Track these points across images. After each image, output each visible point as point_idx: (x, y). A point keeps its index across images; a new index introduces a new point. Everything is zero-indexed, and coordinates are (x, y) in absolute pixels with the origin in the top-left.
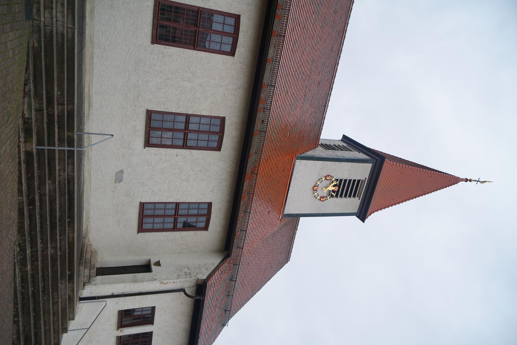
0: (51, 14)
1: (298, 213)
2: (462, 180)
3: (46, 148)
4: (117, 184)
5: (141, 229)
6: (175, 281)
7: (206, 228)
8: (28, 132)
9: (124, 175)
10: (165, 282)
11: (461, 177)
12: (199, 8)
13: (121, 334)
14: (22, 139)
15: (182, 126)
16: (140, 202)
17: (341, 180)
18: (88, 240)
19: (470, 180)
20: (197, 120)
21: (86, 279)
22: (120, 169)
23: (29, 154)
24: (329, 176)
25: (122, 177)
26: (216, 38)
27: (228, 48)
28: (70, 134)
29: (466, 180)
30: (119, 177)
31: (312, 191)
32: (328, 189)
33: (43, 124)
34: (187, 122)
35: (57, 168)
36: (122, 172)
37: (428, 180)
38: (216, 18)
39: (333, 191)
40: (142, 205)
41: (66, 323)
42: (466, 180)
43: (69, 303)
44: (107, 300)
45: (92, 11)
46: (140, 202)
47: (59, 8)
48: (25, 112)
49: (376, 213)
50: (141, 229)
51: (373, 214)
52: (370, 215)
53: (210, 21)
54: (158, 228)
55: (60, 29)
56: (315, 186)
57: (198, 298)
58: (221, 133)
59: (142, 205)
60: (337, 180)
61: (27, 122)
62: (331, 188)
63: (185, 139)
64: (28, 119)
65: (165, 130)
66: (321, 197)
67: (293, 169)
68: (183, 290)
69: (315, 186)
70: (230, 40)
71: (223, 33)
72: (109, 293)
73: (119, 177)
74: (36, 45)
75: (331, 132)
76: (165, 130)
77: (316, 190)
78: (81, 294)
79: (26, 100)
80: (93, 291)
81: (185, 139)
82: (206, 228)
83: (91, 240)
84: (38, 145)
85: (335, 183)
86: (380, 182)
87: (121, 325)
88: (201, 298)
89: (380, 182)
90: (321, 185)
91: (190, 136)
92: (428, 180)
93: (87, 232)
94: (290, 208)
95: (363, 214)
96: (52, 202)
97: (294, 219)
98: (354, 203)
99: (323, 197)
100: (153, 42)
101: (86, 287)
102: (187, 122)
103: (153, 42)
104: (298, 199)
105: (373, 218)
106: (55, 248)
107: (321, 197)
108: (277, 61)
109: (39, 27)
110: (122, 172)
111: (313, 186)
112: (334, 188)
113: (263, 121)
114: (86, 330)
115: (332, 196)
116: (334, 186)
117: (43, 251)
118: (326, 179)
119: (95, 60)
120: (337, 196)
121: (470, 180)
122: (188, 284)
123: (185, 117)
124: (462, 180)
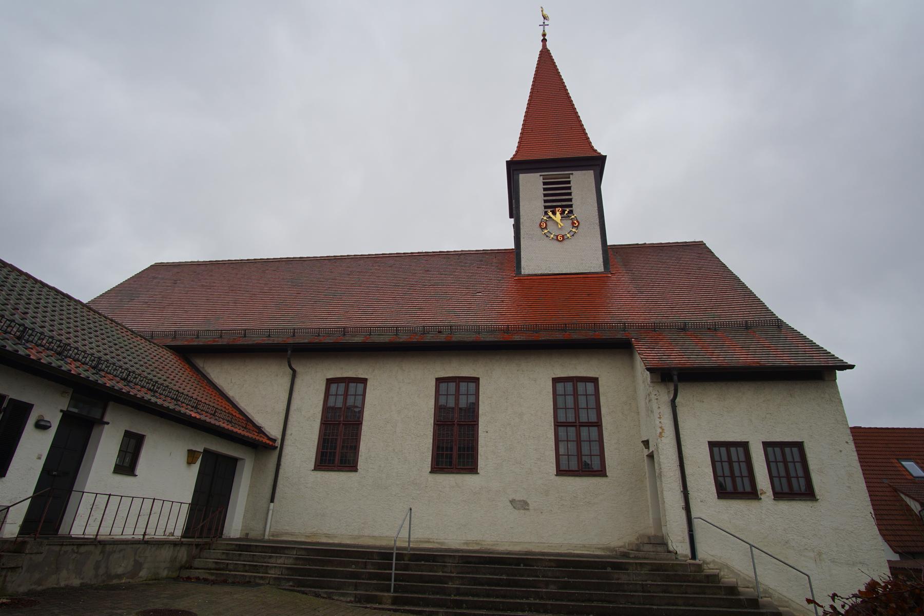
0: (271, 568)
1: (601, 252)
2: (544, 46)
3: (393, 582)
4: (531, 508)
5: (601, 472)
6: (657, 416)
7: (595, 381)
8: (370, 599)
9: (517, 498)
10: (659, 430)
11: (541, 48)
12: (321, 423)
13: (770, 493)
14: (377, 606)
15: (572, 430)
16: (557, 475)
17: (546, 207)
18: (621, 547)
19: (544, 35)
20: (561, 414)
21: (659, 549)
22: (509, 504)
23: (395, 601)
24: (540, 225)
25: (520, 501)
26: (351, 401)
27: (472, 385)
28: (406, 558)
29: (544, 40)
30: (523, 505)
31: (565, 242)
32: (559, 221)
33: (371, 584)
34: (566, 425)
35: (441, 574)
36: (512, 502)
37: (549, 92)
38: (331, 403)
39: (562, 213)
40: (560, 472)
41: (708, 576)
42: (544, 40)
43: (665, 571)
44: (694, 515)
45: (327, 536)
46: (557, 475)
47: (273, 560)
48: (349, 599)
49: (593, 144)
50: (601, 472)
51: (595, 148)
52: (595, 151)
53: (334, 409)
54: (598, 448)
55: (291, 561)
56: (557, 239)
57: (675, 378)
58: (458, 380)
59: (560, 472)
60: (546, 213)
61: (359, 599)
62: (558, 218)
63: (589, 424)
64: (356, 597)
65: (455, 447)
66: (573, 227)
67: (536, 275)
68: (673, 403)
69: (557, 239)
70: (352, 385)
71: (346, 394)
72: (683, 514)
73: (523, 505)
74: (291, 584)
75: (500, 237)
76: (455, 447)
77: (563, 236)
78: (686, 556)
79: (336, 598)
80: (679, 538)
81: (589, 424)
82: (595, 381)
83: (621, 544)
84: (389, 591)
85: (550, 214)
86: (555, 153)
87: (753, 494)
88: (675, 373)
89: (555, 153)
90: (555, 232)
91: (583, 418)
92: (549, 92)
93: (608, 549)
94: (594, 263)
95: (596, 163)
96: (476, 582)
97: (610, 253)
98: (580, 180)
99: (573, 223)
100: (356, 470)
101: (671, 548)
102: (566, 425)
103: (356, 470)
104: (583, 258)
105: (600, 145)
106: (547, 584)
107: (573, 227)
108: (370, 331)
109: (275, 578)
110: (512, 502)
111: (557, 243)
112: (558, 214)
113: (440, 332)
114: (755, 551)
115: (571, 212)
116: (554, 213)
117: (542, 598)
118: (546, 228)
119: (376, 534)
120: (571, 206)
121: (544, 35)
122: (663, 396)
123: (560, 428)
124: (544, 46)
